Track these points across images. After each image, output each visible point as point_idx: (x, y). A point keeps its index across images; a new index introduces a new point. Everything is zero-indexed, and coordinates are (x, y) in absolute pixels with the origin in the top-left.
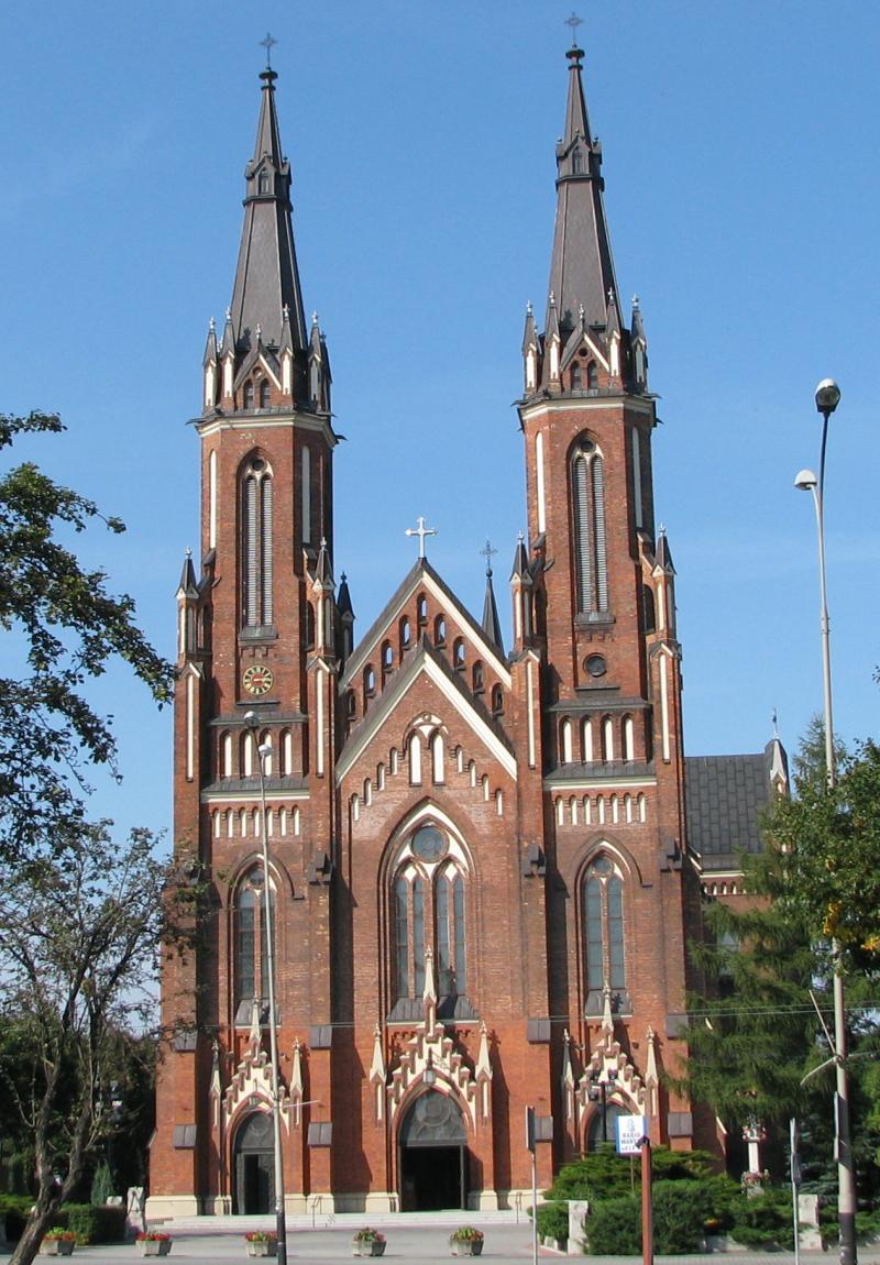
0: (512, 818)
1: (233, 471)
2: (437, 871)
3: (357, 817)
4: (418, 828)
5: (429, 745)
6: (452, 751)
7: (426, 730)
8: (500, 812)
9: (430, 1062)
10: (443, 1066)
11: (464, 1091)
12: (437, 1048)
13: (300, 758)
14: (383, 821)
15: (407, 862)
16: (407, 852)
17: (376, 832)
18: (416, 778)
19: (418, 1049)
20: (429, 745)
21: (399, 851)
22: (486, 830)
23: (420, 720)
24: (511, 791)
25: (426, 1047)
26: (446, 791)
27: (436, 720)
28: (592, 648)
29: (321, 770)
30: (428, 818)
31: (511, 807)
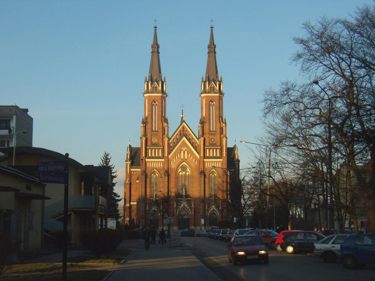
0: (198, 165)
1: (151, 103)
2: (185, 173)
3: (172, 164)
5: (184, 152)
6: (188, 153)
7: (184, 150)
8: (196, 164)
9: (184, 205)
10: (186, 206)
11: (189, 210)
12: (185, 203)
13: (162, 154)
14: (176, 165)
17: (175, 167)
18: (182, 158)
19: (182, 203)
20: (184, 152)
22: (194, 167)
23: (183, 148)
24: (198, 161)
25: (183, 203)
26: (187, 160)
27: (186, 148)
28: (212, 137)
29: (166, 156)
31: (198, 163)
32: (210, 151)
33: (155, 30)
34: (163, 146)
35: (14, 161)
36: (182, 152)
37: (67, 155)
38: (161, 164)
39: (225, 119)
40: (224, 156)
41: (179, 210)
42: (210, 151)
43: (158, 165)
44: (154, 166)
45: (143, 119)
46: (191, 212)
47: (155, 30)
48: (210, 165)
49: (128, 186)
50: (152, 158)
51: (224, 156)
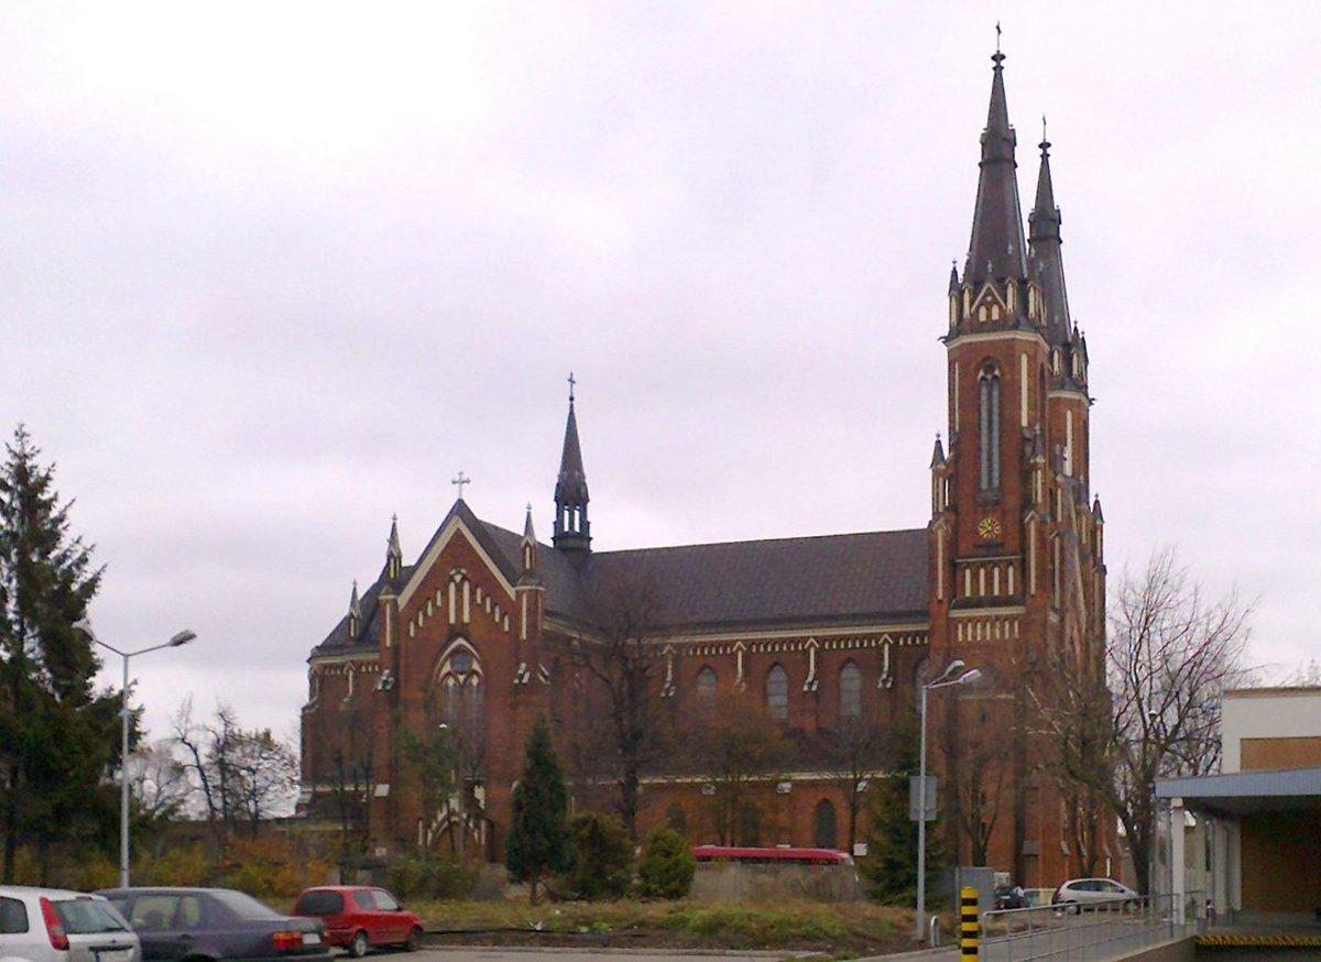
2: (466, 680)
4: (452, 654)
5: (459, 591)
7: (458, 578)
13: (1019, 578)
15: (448, 674)
16: (447, 668)
20: (459, 591)
21: (443, 665)
23: (453, 572)
27: (463, 571)
30: (461, 646)
32: (975, 577)
33: (994, 68)
34: (1024, 550)
35: (524, 619)
36: (452, 587)
37: (591, 539)
38: (1012, 625)
39: (1097, 502)
40: (940, 596)
41: (435, 825)
42: (975, 577)
43: (1003, 633)
44: (984, 637)
45: (955, 272)
46: (476, 835)
47: (994, 68)
48: (993, 634)
49: (468, 936)
50: (977, 603)
51: (940, 596)
